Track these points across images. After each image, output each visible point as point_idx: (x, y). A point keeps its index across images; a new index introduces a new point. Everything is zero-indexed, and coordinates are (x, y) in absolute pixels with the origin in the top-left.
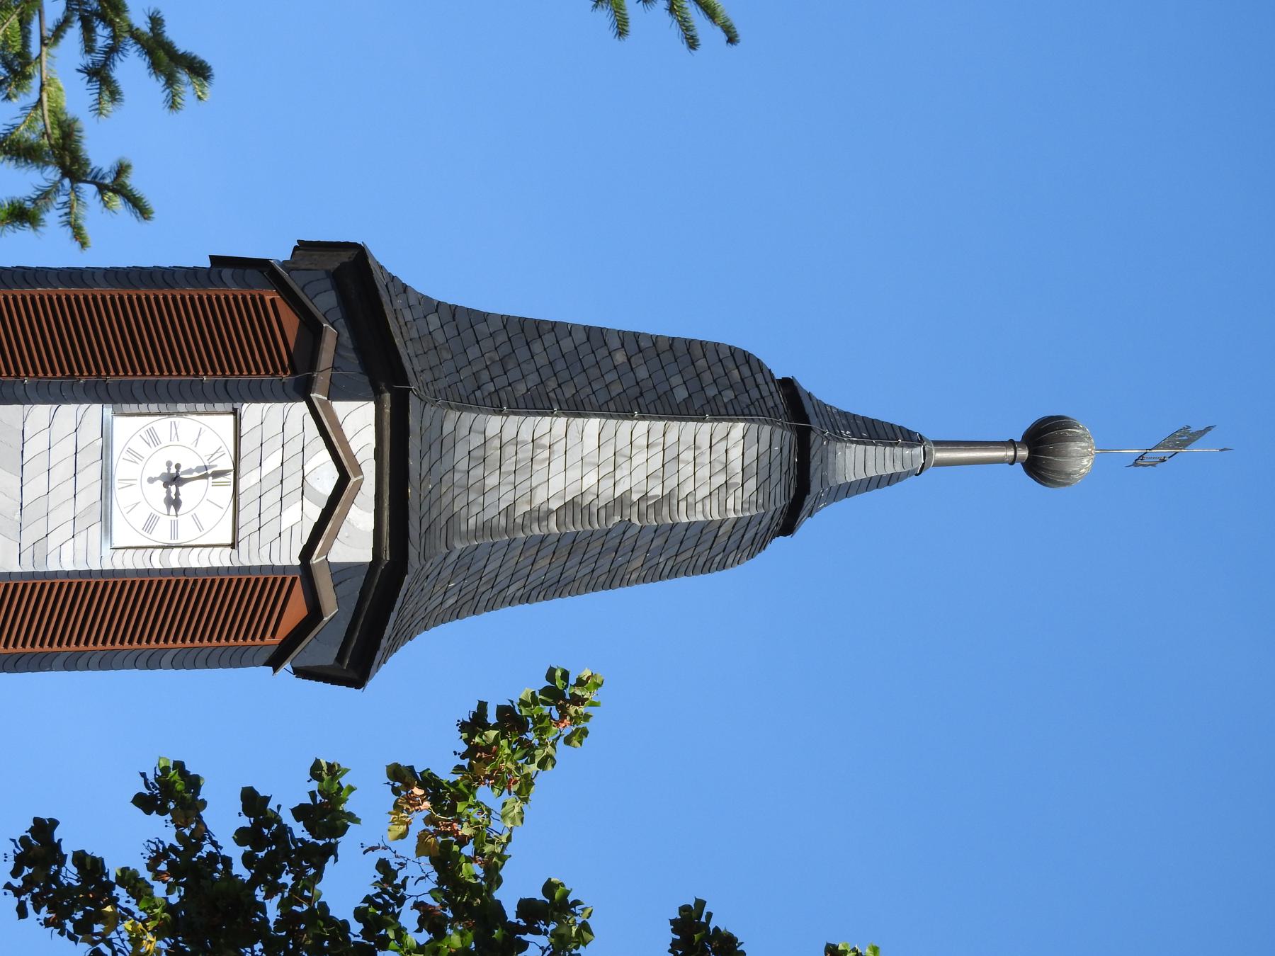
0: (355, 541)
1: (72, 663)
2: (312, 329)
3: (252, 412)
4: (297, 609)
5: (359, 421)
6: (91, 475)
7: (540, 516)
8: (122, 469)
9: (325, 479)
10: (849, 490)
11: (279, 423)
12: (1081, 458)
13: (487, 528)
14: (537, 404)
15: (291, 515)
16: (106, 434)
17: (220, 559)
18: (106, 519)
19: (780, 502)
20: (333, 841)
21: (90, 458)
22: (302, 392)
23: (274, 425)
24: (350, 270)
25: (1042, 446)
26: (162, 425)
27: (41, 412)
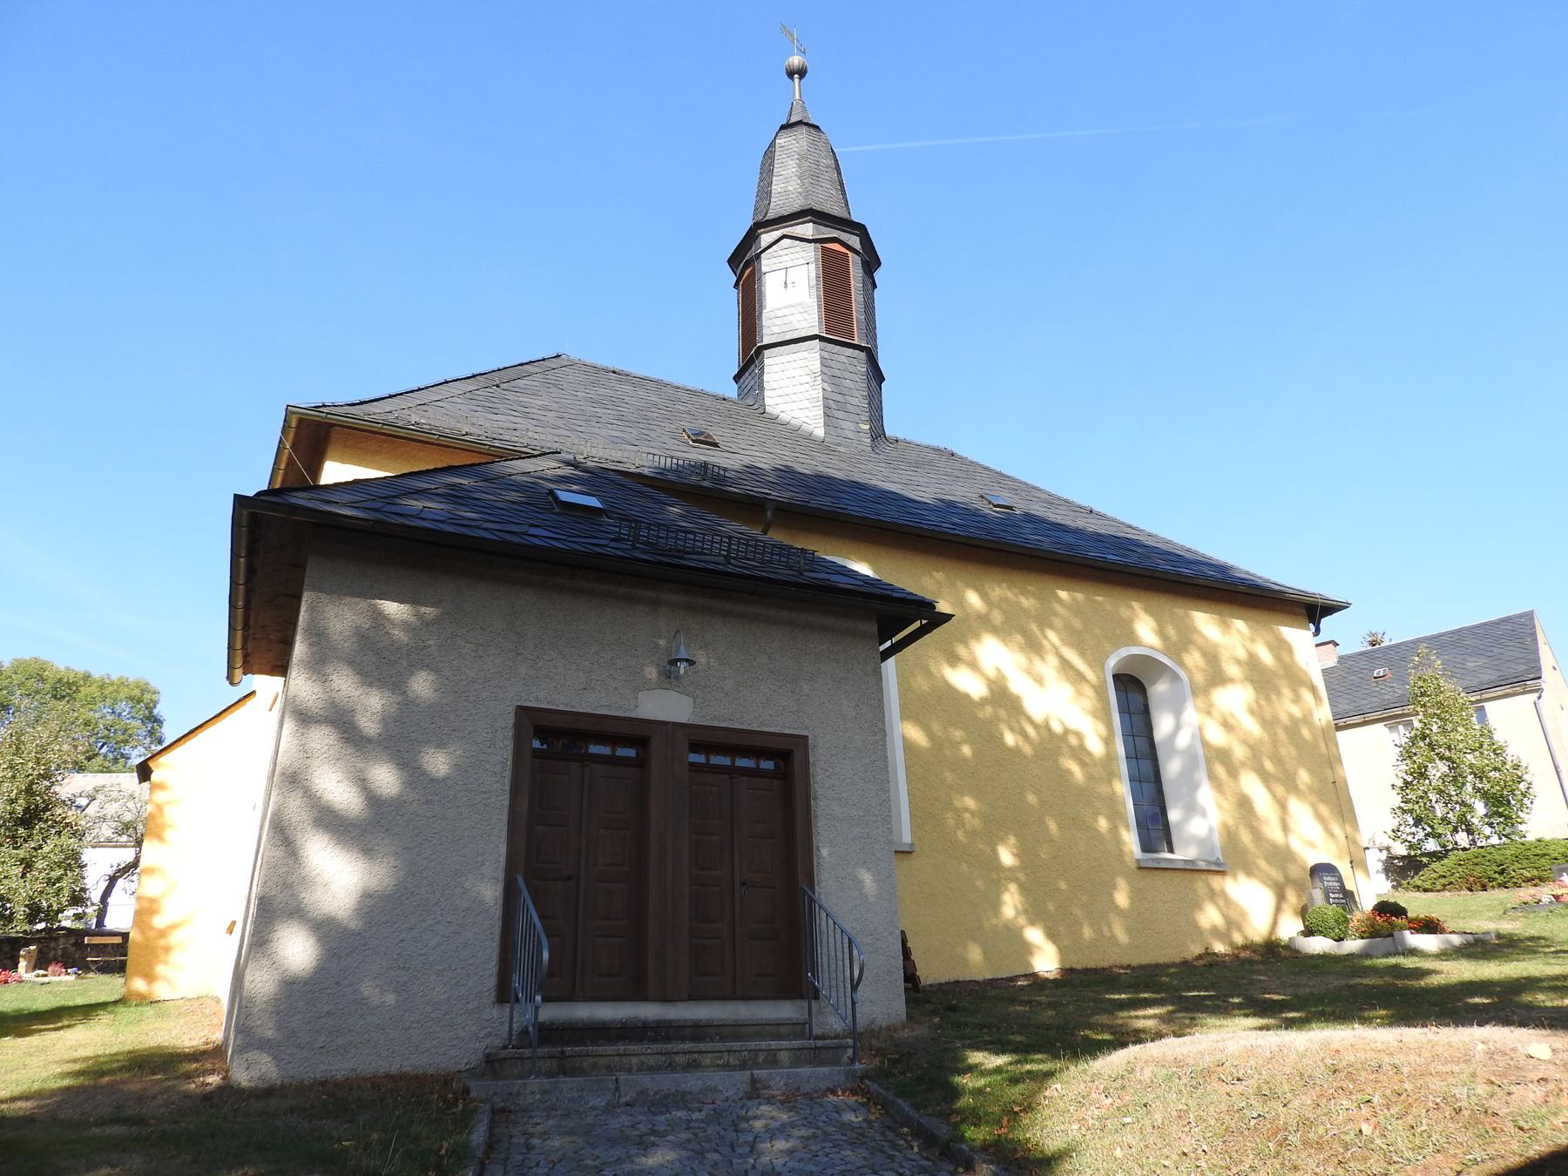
0: (807, 229)
3: (764, 269)
9: (786, 242)
12: (796, 61)
17: (812, 266)
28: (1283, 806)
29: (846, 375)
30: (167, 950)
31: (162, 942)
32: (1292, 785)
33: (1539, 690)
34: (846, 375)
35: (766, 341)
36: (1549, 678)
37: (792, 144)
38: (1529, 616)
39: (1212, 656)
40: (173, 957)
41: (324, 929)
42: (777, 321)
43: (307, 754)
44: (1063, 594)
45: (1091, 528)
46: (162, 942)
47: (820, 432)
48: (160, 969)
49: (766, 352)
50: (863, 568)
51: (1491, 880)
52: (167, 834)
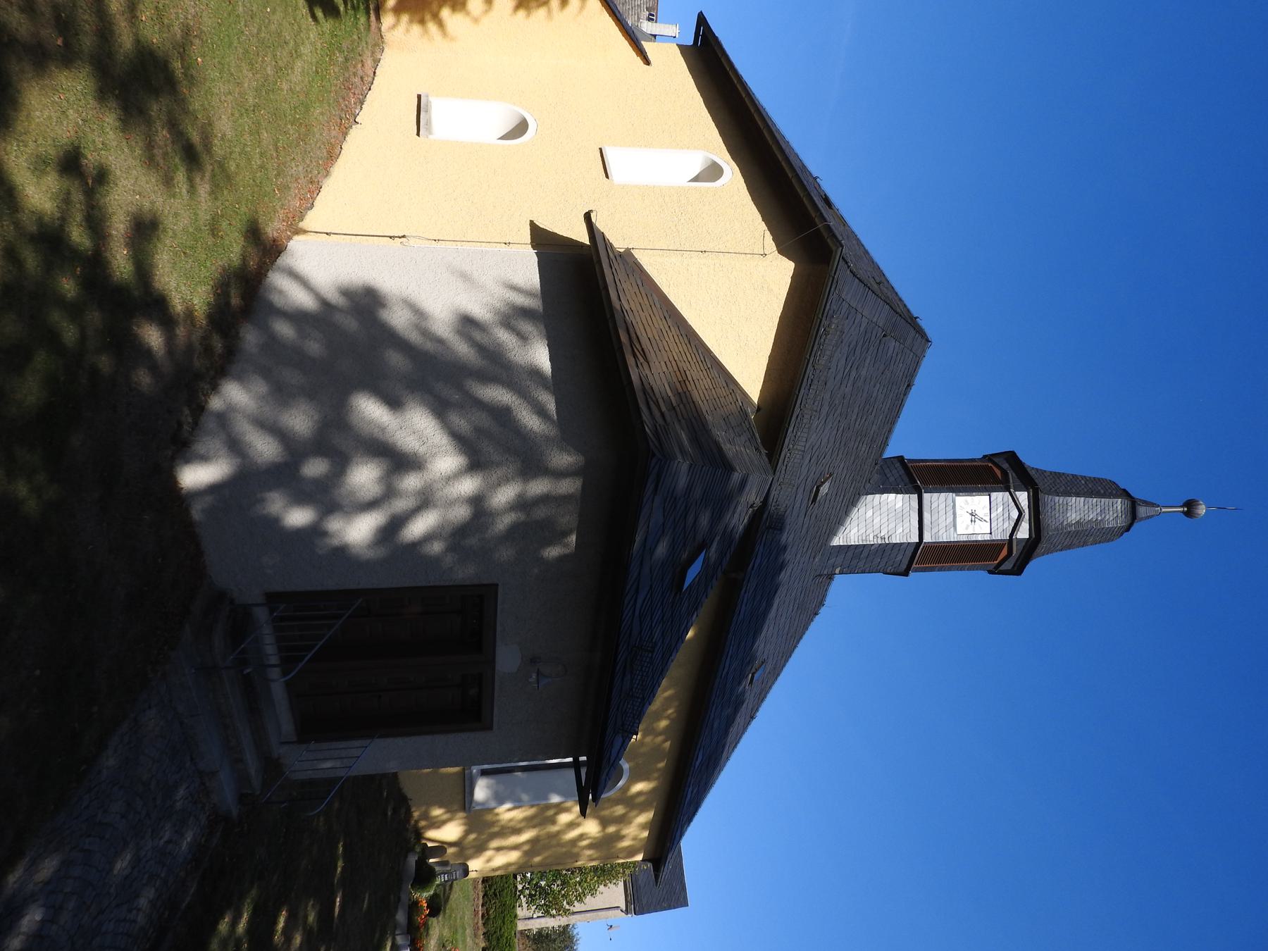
0: (1024, 533)
1: (940, 569)
2: (1004, 473)
3: (994, 495)
4: (1004, 552)
5: (1023, 497)
6: (950, 513)
7: (1070, 525)
8: (958, 511)
9: (1015, 514)
10: (1142, 519)
11: (999, 497)
12: (1202, 510)
13: (1057, 529)
14: (1068, 494)
15: (1006, 525)
16: (954, 502)
17: (987, 538)
18: (955, 526)
19: (1129, 517)
20: (261, 614)
21: (950, 508)
22: (1007, 489)
23: (1000, 499)
24: (1011, 457)
25: (1190, 507)
26: (969, 498)
27: (936, 495)
28: (515, 847)
29: (885, 560)
30: (422, 22)
31: (428, 17)
32: (529, 854)
33: (627, 912)
34: (885, 560)
35: (926, 496)
36: (632, 918)
37: (1114, 510)
38: (685, 904)
39: (623, 820)
40: (416, 29)
41: (315, 532)
42: (942, 506)
43: (451, 503)
44: (668, 744)
45: (738, 720)
46: (428, 17)
47: (837, 541)
48: (405, 18)
49: (915, 496)
50: (690, 634)
51: (490, 887)
52: (521, 13)
